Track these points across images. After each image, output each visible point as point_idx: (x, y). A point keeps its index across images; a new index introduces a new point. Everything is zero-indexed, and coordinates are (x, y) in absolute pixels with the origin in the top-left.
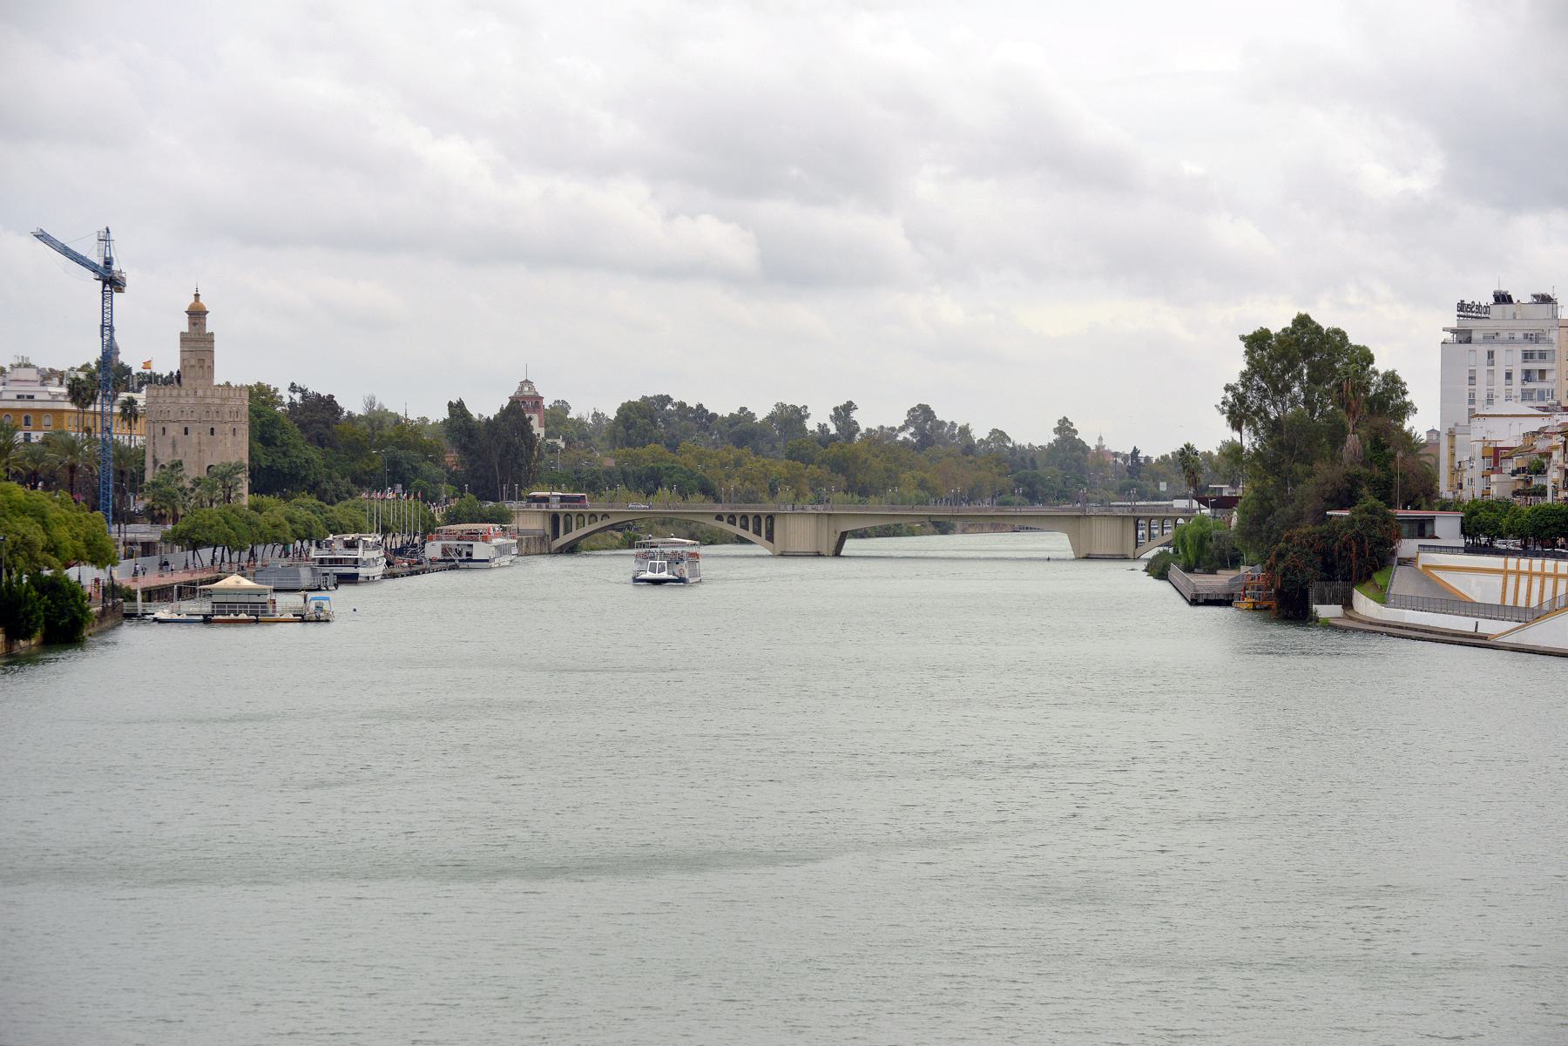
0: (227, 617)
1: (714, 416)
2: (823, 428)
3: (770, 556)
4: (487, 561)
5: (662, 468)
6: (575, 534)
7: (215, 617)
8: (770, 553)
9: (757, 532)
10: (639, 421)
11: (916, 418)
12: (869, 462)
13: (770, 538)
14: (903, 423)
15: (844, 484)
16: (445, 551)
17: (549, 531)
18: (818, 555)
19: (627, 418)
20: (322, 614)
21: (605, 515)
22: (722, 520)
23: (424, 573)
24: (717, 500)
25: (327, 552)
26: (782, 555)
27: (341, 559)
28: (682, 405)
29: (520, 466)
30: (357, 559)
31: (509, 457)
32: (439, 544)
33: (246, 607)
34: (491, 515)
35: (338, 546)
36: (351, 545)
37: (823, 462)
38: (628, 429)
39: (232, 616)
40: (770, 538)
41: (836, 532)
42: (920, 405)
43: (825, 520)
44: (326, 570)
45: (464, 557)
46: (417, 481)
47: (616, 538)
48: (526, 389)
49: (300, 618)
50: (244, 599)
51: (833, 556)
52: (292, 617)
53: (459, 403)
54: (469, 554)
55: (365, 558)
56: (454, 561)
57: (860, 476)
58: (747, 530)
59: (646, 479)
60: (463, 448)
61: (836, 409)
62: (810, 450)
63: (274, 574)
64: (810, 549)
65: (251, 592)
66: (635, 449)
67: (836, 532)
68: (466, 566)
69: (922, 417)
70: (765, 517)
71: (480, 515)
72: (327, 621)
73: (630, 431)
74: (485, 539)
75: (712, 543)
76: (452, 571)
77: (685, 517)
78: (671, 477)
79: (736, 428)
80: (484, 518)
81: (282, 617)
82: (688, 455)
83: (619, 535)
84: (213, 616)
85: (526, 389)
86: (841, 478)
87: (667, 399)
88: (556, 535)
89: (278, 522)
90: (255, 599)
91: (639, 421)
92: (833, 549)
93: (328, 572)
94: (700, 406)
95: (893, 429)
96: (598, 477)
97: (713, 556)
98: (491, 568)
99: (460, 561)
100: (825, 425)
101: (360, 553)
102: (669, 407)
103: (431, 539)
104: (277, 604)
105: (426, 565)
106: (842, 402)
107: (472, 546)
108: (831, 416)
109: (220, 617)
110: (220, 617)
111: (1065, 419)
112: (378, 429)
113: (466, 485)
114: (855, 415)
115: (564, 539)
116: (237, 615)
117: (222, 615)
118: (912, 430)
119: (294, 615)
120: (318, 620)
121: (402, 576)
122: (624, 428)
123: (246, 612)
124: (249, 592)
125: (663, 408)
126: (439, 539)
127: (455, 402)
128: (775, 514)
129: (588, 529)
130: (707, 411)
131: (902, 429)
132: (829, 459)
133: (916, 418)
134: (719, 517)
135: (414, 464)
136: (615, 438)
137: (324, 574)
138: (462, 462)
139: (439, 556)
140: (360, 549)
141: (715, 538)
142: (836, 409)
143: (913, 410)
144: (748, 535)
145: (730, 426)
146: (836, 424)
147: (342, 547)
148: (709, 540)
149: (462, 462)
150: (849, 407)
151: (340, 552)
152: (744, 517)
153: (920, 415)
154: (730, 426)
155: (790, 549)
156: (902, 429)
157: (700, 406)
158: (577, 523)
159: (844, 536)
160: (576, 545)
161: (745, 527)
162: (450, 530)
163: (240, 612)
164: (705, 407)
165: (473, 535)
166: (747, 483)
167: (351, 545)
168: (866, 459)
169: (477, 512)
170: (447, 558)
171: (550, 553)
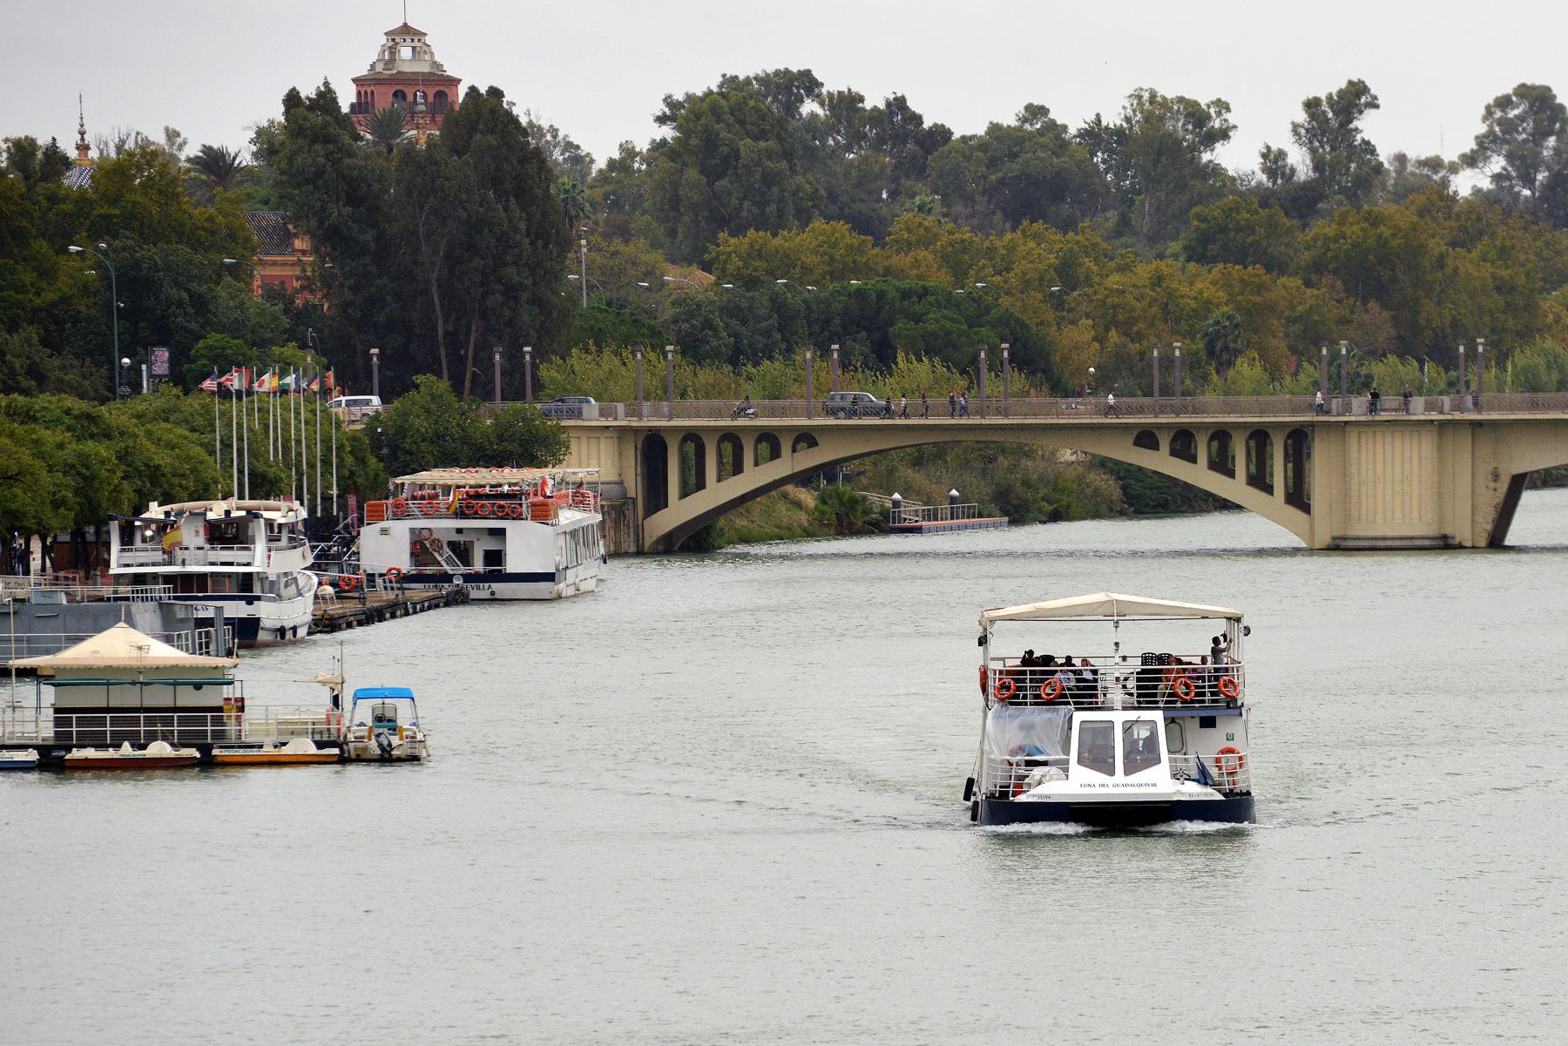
0: (110, 753)
1: (942, 134)
2: (1274, 161)
3: (1295, 551)
4: (549, 577)
5: (892, 294)
6: (717, 492)
7: (76, 754)
8: (1304, 545)
9: (1260, 481)
10: (746, 145)
11: (1509, 126)
12: (1450, 261)
13: (1298, 498)
14: (1469, 145)
15: (1386, 332)
16: (421, 548)
17: (634, 486)
18: (1445, 545)
19: (711, 143)
20: (395, 741)
21: (806, 438)
22: (1157, 449)
23: (393, 616)
24: (1059, 388)
25: (159, 556)
26: (1339, 546)
27: (202, 577)
28: (847, 103)
29: (511, 292)
30: (250, 574)
31: (477, 261)
32: (401, 530)
33: (169, 722)
34: (501, 438)
35: (191, 535)
36: (226, 534)
37: (1318, 266)
38: (713, 175)
39: (126, 750)
40: (1298, 498)
41: (1496, 476)
42: (1523, 86)
43: (1465, 440)
44: (206, 610)
45: (479, 566)
46: (213, 338)
47: (798, 505)
48: (406, 52)
49: (336, 751)
50: (159, 697)
51: (1486, 547)
52: (313, 750)
53: (320, 95)
54: (494, 557)
55: (272, 573)
56: (447, 578)
57: (1429, 307)
58: (1231, 474)
59: (844, 327)
60: (331, 239)
61: (1312, 105)
62: (1260, 231)
63: (53, 622)
64: (1421, 526)
65: (181, 677)
66: (774, 235)
67: (1496, 476)
68: (485, 594)
69: (1529, 125)
70: (717, 436)
71: (465, 440)
72: (414, 759)
73: (723, 183)
74: (542, 513)
75: (1056, 517)
76: (450, 610)
77: (991, 437)
78: (917, 319)
79: (1013, 169)
80: (480, 448)
81: (285, 750)
82: (922, 254)
83: (807, 497)
84: (69, 749)
85: (406, 52)
86: (1376, 314)
87: (807, 83)
88: (656, 498)
89: (14, 469)
90: (188, 698)
91: (746, 145)
92: (1489, 527)
93: (210, 614)
94: (899, 104)
95: (1434, 164)
96: (708, 324)
97: (947, 555)
98: (559, 597)
99: (468, 578)
100: (1281, 154)
101: (259, 558)
102: (809, 107)
103: (378, 516)
104: (246, 715)
105: (382, 595)
106: (1329, 85)
107: (500, 533)
108: (1295, 128)
109: (90, 753)
110: (90, 753)
111: (294, 89)
112: (41, 180)
113: (375, 351)
114: (1368, 126)
115: (680, 511)
116: (144, 747)
117: (97, 747)
118: (1497, 164)
119: (320, 745)
120: (386, 758)
121: (349, 626)
122: (702, 172)
123: (166, 737)
124: (172, 677)
125: (792, 106)
126: (401, 514)
127: (308, 91)
128: (1312, 425)
129: (754, 477)
130: (918, 119)
131: (1471, 160)
132: (1336, 258)
133: (1509, 126)
134: (1146, 438)
135: (194, 286)
136: (675, 202)
137: (202, 623)
138: (327, 280)
139: (405, 565)
140: (260, 546)
141: (1066, 500)
142: (1312, 105)
143: (1504, 102)
144: (1233, 488)
145: (993, 163)
146: (1313, 151)
147: (201, 540)
148: (1048, 508)
149: (327, 280)
150: (1354, 98)
151: (199, 560)
152: (1221, 435)
153: (1521, 118)
154: (993, 163)
155: (1362, 530)
156: (1471, 160)
157: (899, 104)
158: (720, 463)
159: (1518, 485)
160: (708, 530)
161: (1222, 465)
162: (421, 487)
163: (152, 737)
164: (914, 105)
165: (508, 504)
166: (1114, 336)
167: (226, 534)
168: (1442, 257)
169: (456, 432)
170: (429, 570)
171: (640, 553)
